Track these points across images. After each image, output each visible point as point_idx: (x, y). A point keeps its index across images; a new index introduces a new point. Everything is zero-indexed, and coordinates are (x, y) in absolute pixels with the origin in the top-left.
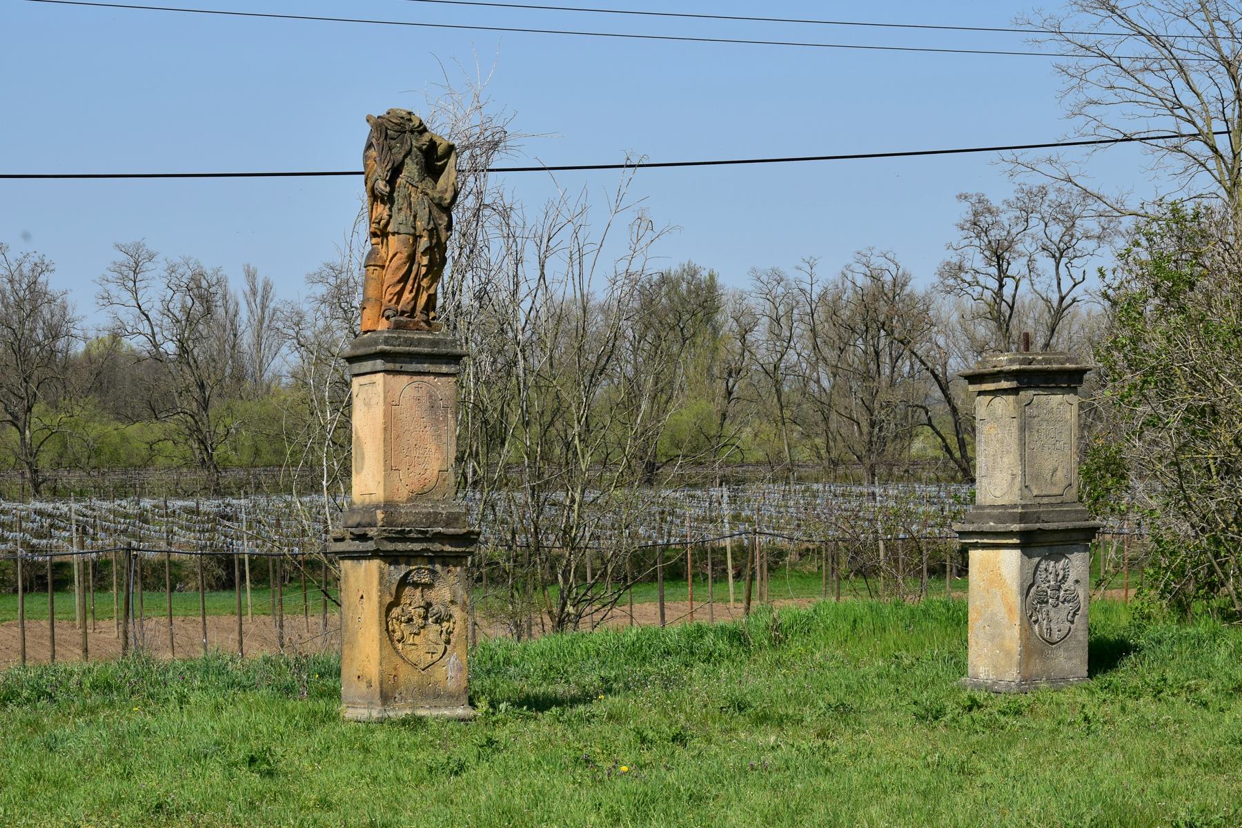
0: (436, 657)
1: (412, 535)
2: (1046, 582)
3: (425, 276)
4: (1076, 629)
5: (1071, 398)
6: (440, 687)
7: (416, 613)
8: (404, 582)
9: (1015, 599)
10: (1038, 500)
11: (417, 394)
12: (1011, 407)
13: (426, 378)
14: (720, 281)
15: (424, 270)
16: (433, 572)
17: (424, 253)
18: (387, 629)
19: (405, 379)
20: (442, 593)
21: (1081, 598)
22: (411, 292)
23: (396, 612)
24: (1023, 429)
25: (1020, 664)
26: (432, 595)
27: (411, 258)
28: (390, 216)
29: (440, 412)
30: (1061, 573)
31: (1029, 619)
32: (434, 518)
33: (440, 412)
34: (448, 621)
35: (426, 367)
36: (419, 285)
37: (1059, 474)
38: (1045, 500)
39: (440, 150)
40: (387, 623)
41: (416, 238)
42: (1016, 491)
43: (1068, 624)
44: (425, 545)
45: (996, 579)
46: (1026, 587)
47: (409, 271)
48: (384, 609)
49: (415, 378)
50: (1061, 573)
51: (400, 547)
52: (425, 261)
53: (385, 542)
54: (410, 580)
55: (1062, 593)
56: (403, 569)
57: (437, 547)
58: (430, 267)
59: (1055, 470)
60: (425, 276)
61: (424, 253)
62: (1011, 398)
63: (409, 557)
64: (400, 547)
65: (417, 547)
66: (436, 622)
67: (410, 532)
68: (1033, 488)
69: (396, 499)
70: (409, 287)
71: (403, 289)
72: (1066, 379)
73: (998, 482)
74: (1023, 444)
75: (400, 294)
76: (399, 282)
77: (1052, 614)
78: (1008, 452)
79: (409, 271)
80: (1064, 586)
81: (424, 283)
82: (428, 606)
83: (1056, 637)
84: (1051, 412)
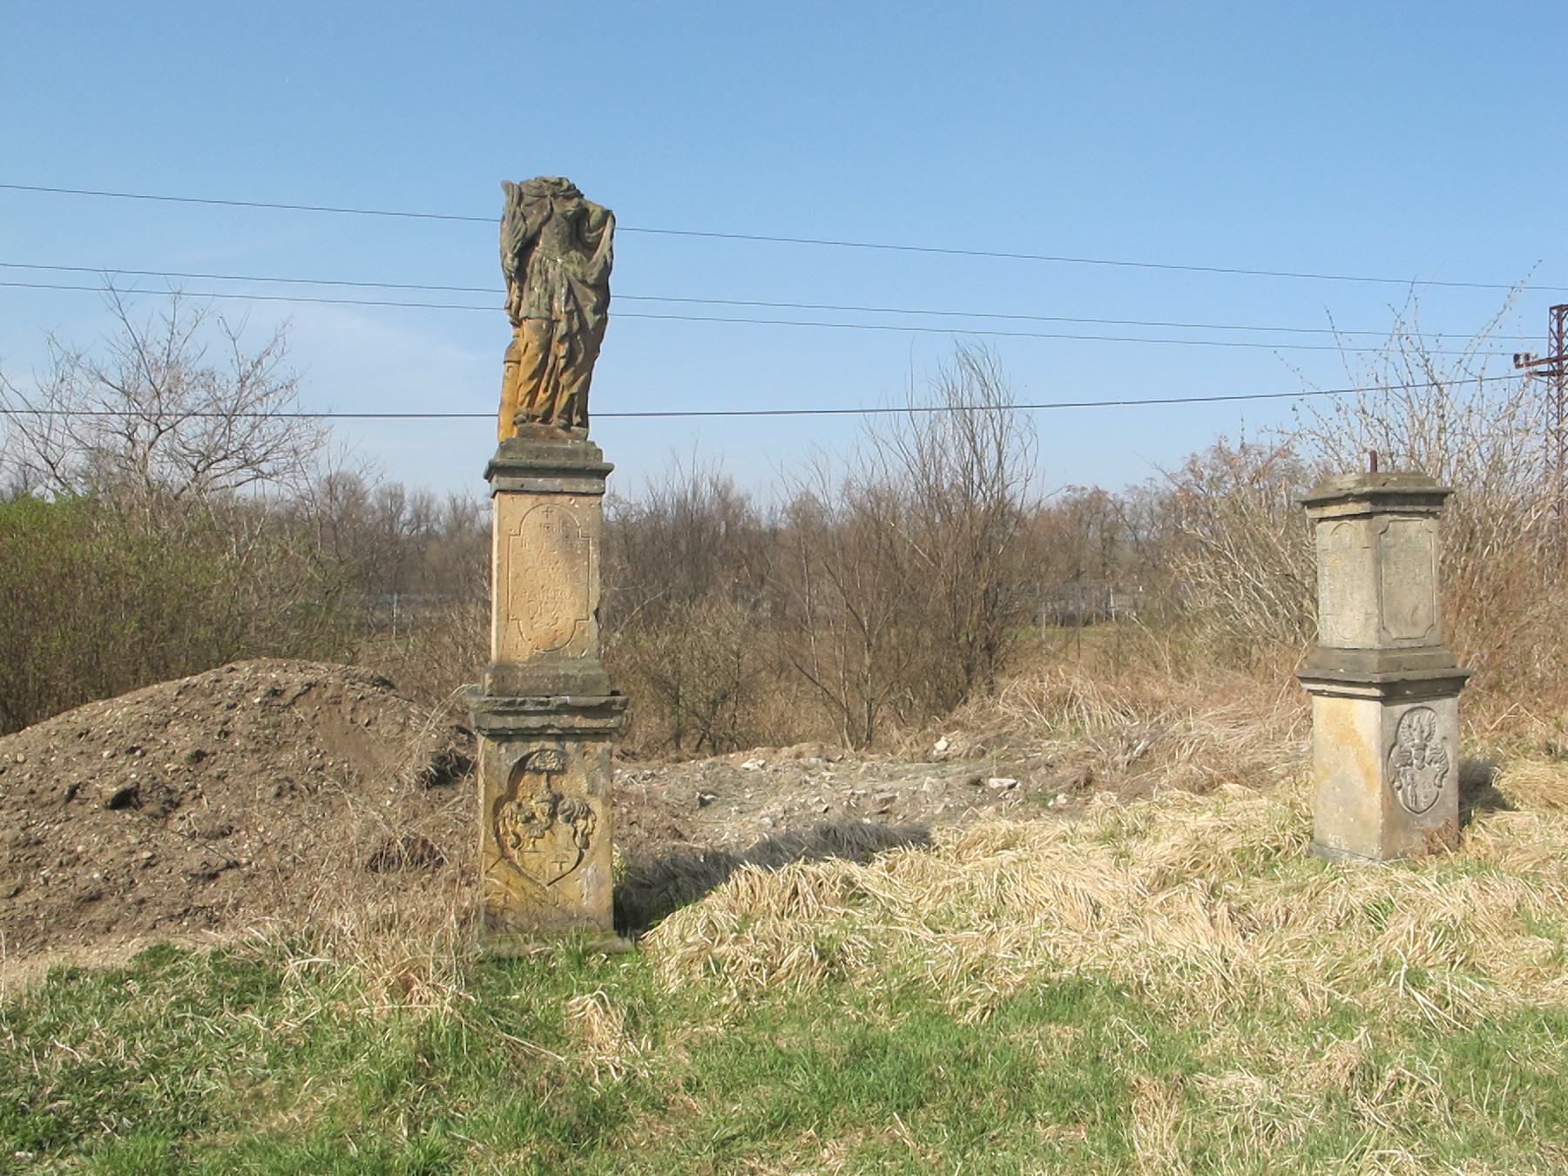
0: (567, 867)
1: (529, 707)
2: (1410, 740)
3: (565, 369)
4: (1445, 795)
5: (1430, 523)
6: (571, 906)
7: (537, 805)
8: (521, 767)
9: (1376, 764)
10: (1398, 644)
11: (544, 521)
12: (1363, 536)
13: (559, 499)
14: (740, 488)
15: (562, 363)
16: (562, 754)
17: (561, 341)
18: (497, 834)
19: (528, 500)
20: (575, 785)
21: (1450, 756)
22: (546, 390)
23: (508, 808)
24: (1378, 561)
25: (1382, 839)
26: (563, 784)
27: (546, 348)
28: (521, 298)
29: (579, 543)
30: (1427, 729)
31: (1391, 786)
32: (566, 684)
33: (579, 543)
34: (586, 818)
35: (557, 483)
36: (557, 383)
37: (1421, 613)
38: (1406, 644)
39: (594, 219)
40: (496, 824)
41: (552, 323)
42: (1372, 632)
43: (1435, 789)
44: (545, 720)
45: (1348, 735)
46: (1387, 747)
47: (545, 358)
48: (491, 806)
49: (543, 499)
50: (1427, 729)
51: (511, 722)
52: (563, 351)
53: (489, 717)
54: (529, 765)
55: (1428, 752)
56: (520, 749)
57: (565, 720)
58: (571, 357)
59: (1416, 609)
60: (565, 369)
61: (561, 341)
62: (1363, 523)
63: (528, 735)
64: (511, 722)
65: (534, 722)
66: (568, 820)
67: (523, 703)
68: (1391, 630)
69: (513, 657)
70: (543, 385)
71: (537, 387)
72: (1428, 500)
73: (1347, 620)
74: (1378, 578)
75: (533, 393)
76: (531, 378)
77: (1417, 777)
78: (1359, 587)
79: (545, 358)
80: (1431, 744)
81: (565, 379)
82: (557, 799)
83: (1423, 806)
84: (1409, 540)
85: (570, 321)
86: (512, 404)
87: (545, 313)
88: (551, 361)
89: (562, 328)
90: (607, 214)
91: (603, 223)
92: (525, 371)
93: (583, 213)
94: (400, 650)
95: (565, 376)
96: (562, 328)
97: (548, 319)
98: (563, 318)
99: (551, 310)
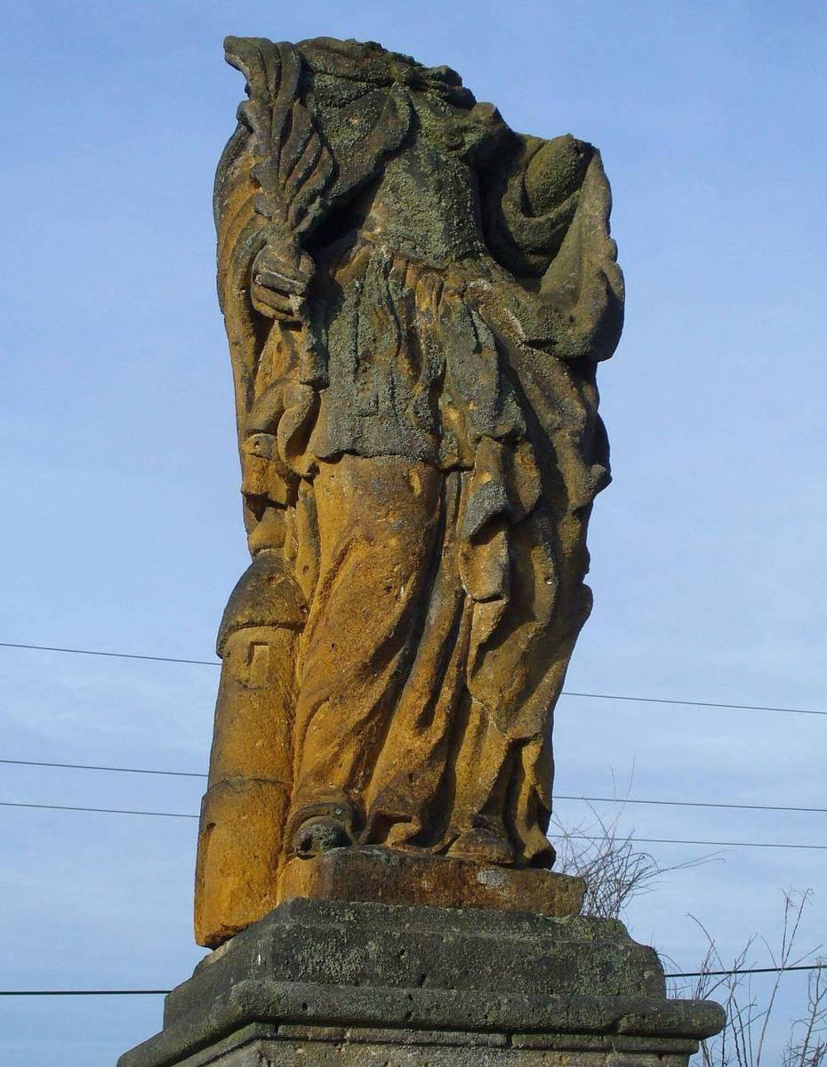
15: (483, 619)
22: (425, 721)
36: (462, 698)
41: (441, 473)
47: (419, 603)
71: (386, 708)
79: (419, 603)
85: (507, 470)
86: (278, 785)
87: (423, 441)
88: (438, 611)
89: (479, 495)
90: (585, 154)
91: (575, 180)
92: (322, 659)
93: (500, 151)
94: (578, 1060)
95: (490, 672)
96: (479, 495)
97: (431, 459)
98: (485, 456)
99: (436, 428)
